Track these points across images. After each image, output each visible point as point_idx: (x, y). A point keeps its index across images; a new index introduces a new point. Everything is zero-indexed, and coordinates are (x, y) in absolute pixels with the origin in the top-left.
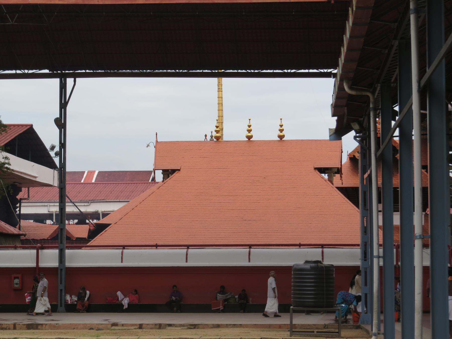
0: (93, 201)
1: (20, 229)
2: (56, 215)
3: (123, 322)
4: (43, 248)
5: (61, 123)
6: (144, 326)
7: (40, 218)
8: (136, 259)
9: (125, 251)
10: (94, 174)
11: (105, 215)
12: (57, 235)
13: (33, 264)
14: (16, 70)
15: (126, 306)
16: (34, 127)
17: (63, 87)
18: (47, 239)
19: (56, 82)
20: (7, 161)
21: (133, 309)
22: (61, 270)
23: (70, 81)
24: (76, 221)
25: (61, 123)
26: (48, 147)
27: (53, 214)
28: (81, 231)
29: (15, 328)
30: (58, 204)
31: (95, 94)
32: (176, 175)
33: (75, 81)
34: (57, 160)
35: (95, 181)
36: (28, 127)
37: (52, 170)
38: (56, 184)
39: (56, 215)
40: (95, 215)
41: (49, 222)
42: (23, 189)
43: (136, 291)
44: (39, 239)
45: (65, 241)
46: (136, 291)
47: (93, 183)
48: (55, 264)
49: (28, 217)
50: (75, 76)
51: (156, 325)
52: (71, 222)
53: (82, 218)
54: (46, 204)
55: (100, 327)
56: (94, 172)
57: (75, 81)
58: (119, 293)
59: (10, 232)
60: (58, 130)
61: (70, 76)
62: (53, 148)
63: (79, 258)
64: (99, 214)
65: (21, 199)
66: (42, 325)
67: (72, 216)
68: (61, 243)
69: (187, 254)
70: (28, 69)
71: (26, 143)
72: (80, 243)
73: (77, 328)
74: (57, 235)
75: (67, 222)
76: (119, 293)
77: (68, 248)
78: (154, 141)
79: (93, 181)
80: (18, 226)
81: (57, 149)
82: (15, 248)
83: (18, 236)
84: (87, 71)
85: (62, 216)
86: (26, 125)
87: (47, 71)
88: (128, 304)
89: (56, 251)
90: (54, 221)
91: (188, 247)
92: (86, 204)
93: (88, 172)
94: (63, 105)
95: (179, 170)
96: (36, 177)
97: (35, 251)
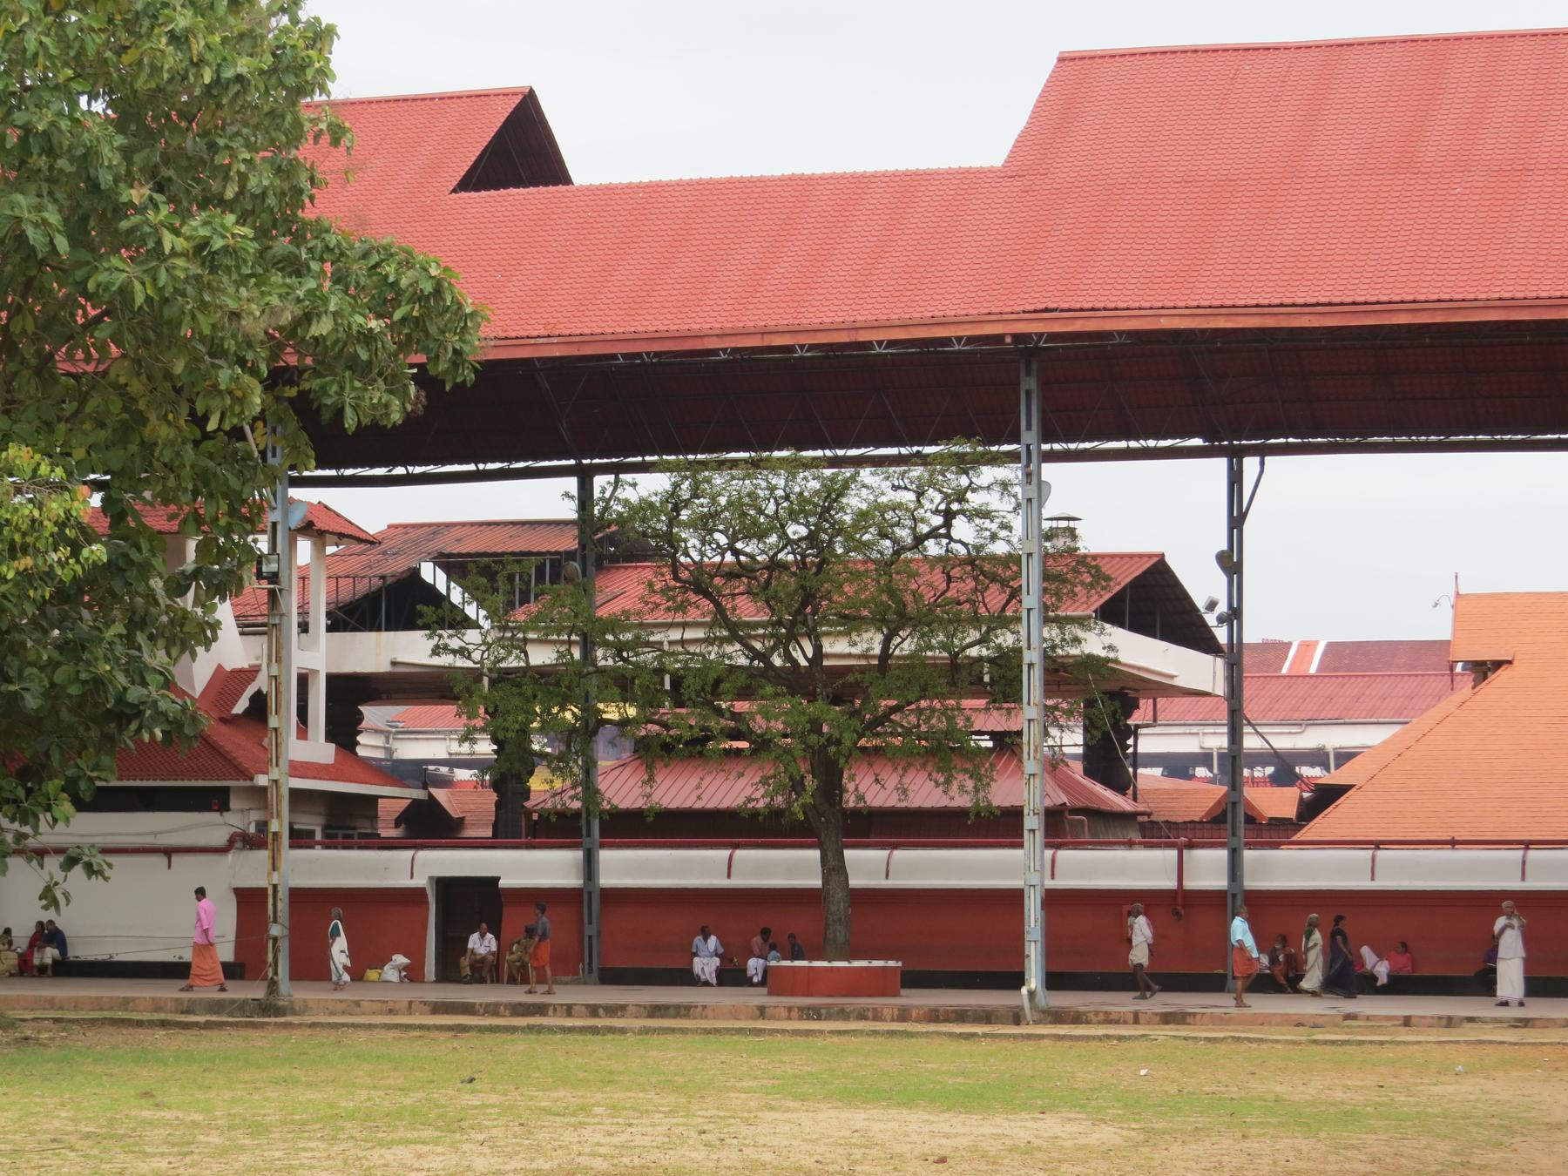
0: (1313, 722)
1: (1135, 799)
2: (1221, 756)
3: (1370, 1012)
4: (1191, 846)
5: (1231, 563)
6: (1414, 1021)
7: (1178, 766)
8: (1405, 872)
9: (1380, 853)
10: (1314, 650)
11: (1344, 757)
12: (1225, 812)
13: (1170, 884)
14: (1128, 439)
15: (1383, 980)
16: (1168, 560)
17: (1235, 479)
18: (1201, 822)
19: (1220, 465)
20: (1112, 655)
21: (1399, 986)
22: (1234, 896)
23: (1250, 464)
24: (1270, 770)
25: (1231, 563)
26: (1200, 604)
27: (1211, 755)
28: (1280, 803)
29: (1136, 1021)
30: (1225, 729)
31: (1305, 490)
32: (1502, 673)
33: (1262, 464)
34: (1221, 635)
35: (1320, 669)
36: (1155, 560)
37: (1209, 658)
38: (1220, 688)
39: (1221, 756)
40: (1318, 757)
41: (1201, 772)
42: (1142, 702)
43: (1404, 945)
44: (1180, 820)
45: (1241, 831)
46: (1404, 945)
47: (1311, 677)
48: (1220, 882)
49: (1154, 760)
50: (1263, 452)
51: (1440, 1018)
52: (1258, 772)
53: (1284, 768)
54: (1194, 730)
55: (1319, 1021)
56: (1315, 644)
57: (1262, 464)
58: (1366, 951)
59: (1116, 809)
60: (1224, 579)
61: (1252, 450)
62: (1212, 606)
63: (1278, 869)
64: (1327, 755)
65: (1137, 727)
66: (1194, 1014)
67: (1258, 759)
68: (1234, 834)
69: (1524, 863)
70: (1157, 438)
71: (1153, 600)
72: (1278, 832)
73: (1270, 1024)
74: (1225, 812)
75: (1246, 772)
76: (1366, 951)
77: (1250, 846)
78: (1452, 595)
79: (1313, 670)
80: (1130, 791)
81: (1222, 608)
82: (1130, 845)
83: (1132, 816)
84: (1291, 440)
85: (1234, 760)
86: (1150, 556)
87: (1197, 442)
88: (1389, 976)
89: (1222, 854)
90: (1215, 770)
91: (1527, 845)
92: (1294, 729)
93: (1300, 645)
94: (1236, 521)
95: (1510, 662)
96: (1172, 677)
97: (1174, 853)
